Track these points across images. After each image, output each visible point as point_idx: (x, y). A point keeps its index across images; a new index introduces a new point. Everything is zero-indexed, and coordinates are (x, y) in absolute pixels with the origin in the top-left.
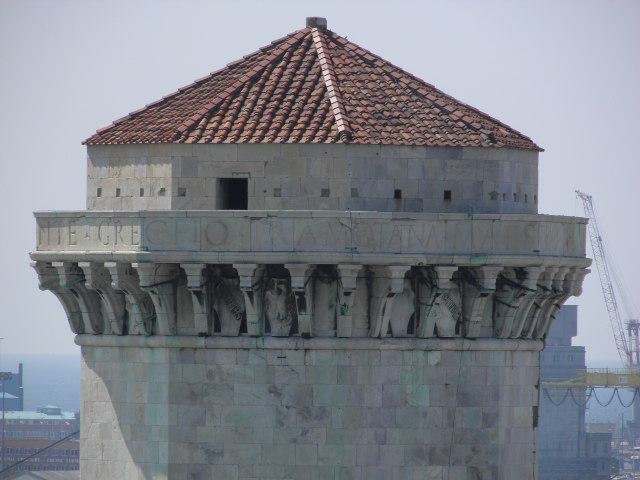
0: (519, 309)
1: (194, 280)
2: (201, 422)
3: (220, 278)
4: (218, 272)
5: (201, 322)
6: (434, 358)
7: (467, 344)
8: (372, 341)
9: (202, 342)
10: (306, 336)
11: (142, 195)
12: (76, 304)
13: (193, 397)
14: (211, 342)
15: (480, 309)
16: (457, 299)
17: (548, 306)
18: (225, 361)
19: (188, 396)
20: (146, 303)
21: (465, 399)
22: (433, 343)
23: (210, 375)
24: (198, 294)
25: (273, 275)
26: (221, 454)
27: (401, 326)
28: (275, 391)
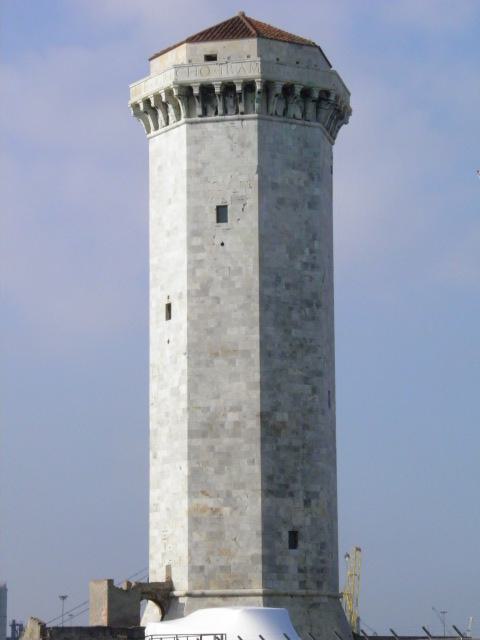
0: (326, 112)
1: (196, 91)
2: (198, 152)
3: (207, 90)
4: (197, 241)
5: (199, 111)
6: (294, 127)
7: (307, 123)
8: (230, 404)
9: (200, 119)
10: (242, 113)
11: (169, 316)
12: (147, 119)
13: (196, 142)
14: (203, 119)
15: (311, 107)
16: (302, 104)
17: (337, 119)
18: (209, 127)
19: (193, 142)
20: (177, 109)
21: (306, 145)
22: (294, 120)
23: (203, 133)
24: (198, 97)
25: (228, 87)
26: (208, 163)
27: (280, 113)
28: (230, 137)
